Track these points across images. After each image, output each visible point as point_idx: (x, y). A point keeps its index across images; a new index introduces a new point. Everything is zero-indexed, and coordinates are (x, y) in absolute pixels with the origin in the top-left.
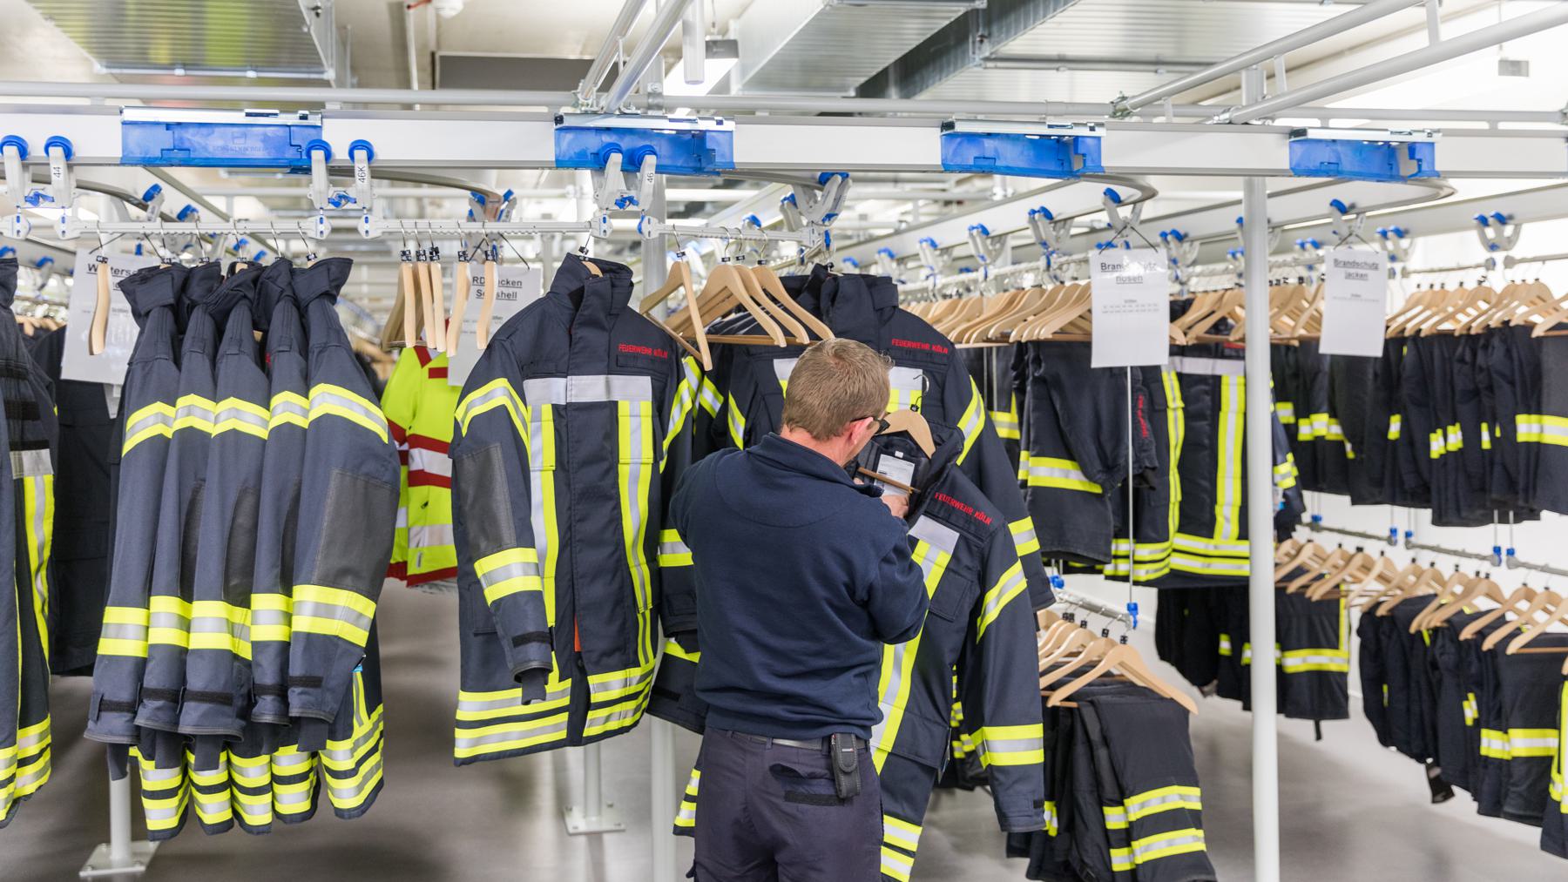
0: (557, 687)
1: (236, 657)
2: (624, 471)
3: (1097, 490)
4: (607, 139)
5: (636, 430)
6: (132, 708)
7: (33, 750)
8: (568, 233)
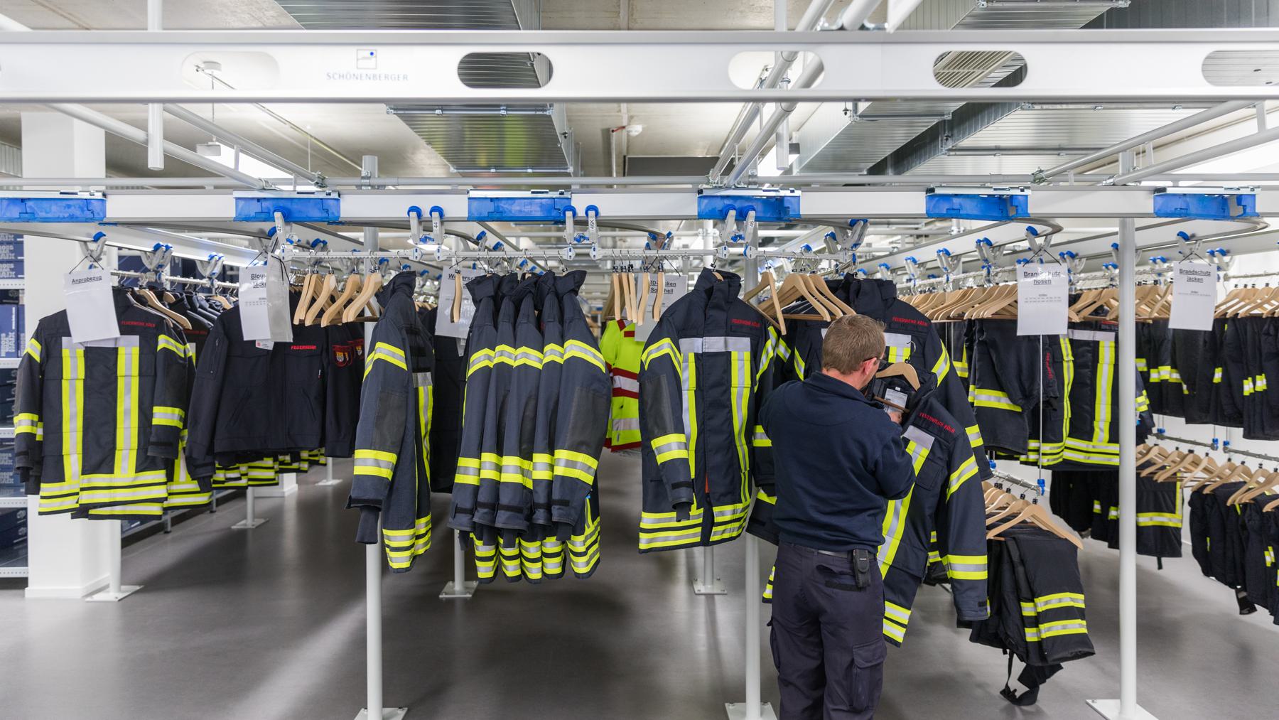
0: (695, 511)
1: (524, 487)
2: (734, 391)
3: (1019, 410)
4: (727, 202)
5: (741, 368)
6: (472, 512)
7: (423, 531)
8: (700, 256)
